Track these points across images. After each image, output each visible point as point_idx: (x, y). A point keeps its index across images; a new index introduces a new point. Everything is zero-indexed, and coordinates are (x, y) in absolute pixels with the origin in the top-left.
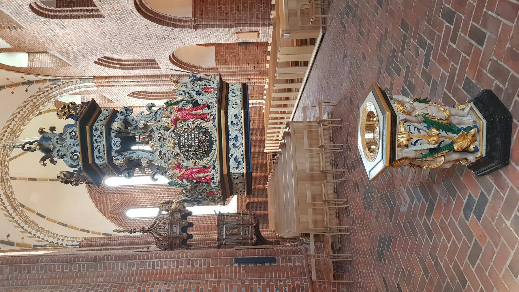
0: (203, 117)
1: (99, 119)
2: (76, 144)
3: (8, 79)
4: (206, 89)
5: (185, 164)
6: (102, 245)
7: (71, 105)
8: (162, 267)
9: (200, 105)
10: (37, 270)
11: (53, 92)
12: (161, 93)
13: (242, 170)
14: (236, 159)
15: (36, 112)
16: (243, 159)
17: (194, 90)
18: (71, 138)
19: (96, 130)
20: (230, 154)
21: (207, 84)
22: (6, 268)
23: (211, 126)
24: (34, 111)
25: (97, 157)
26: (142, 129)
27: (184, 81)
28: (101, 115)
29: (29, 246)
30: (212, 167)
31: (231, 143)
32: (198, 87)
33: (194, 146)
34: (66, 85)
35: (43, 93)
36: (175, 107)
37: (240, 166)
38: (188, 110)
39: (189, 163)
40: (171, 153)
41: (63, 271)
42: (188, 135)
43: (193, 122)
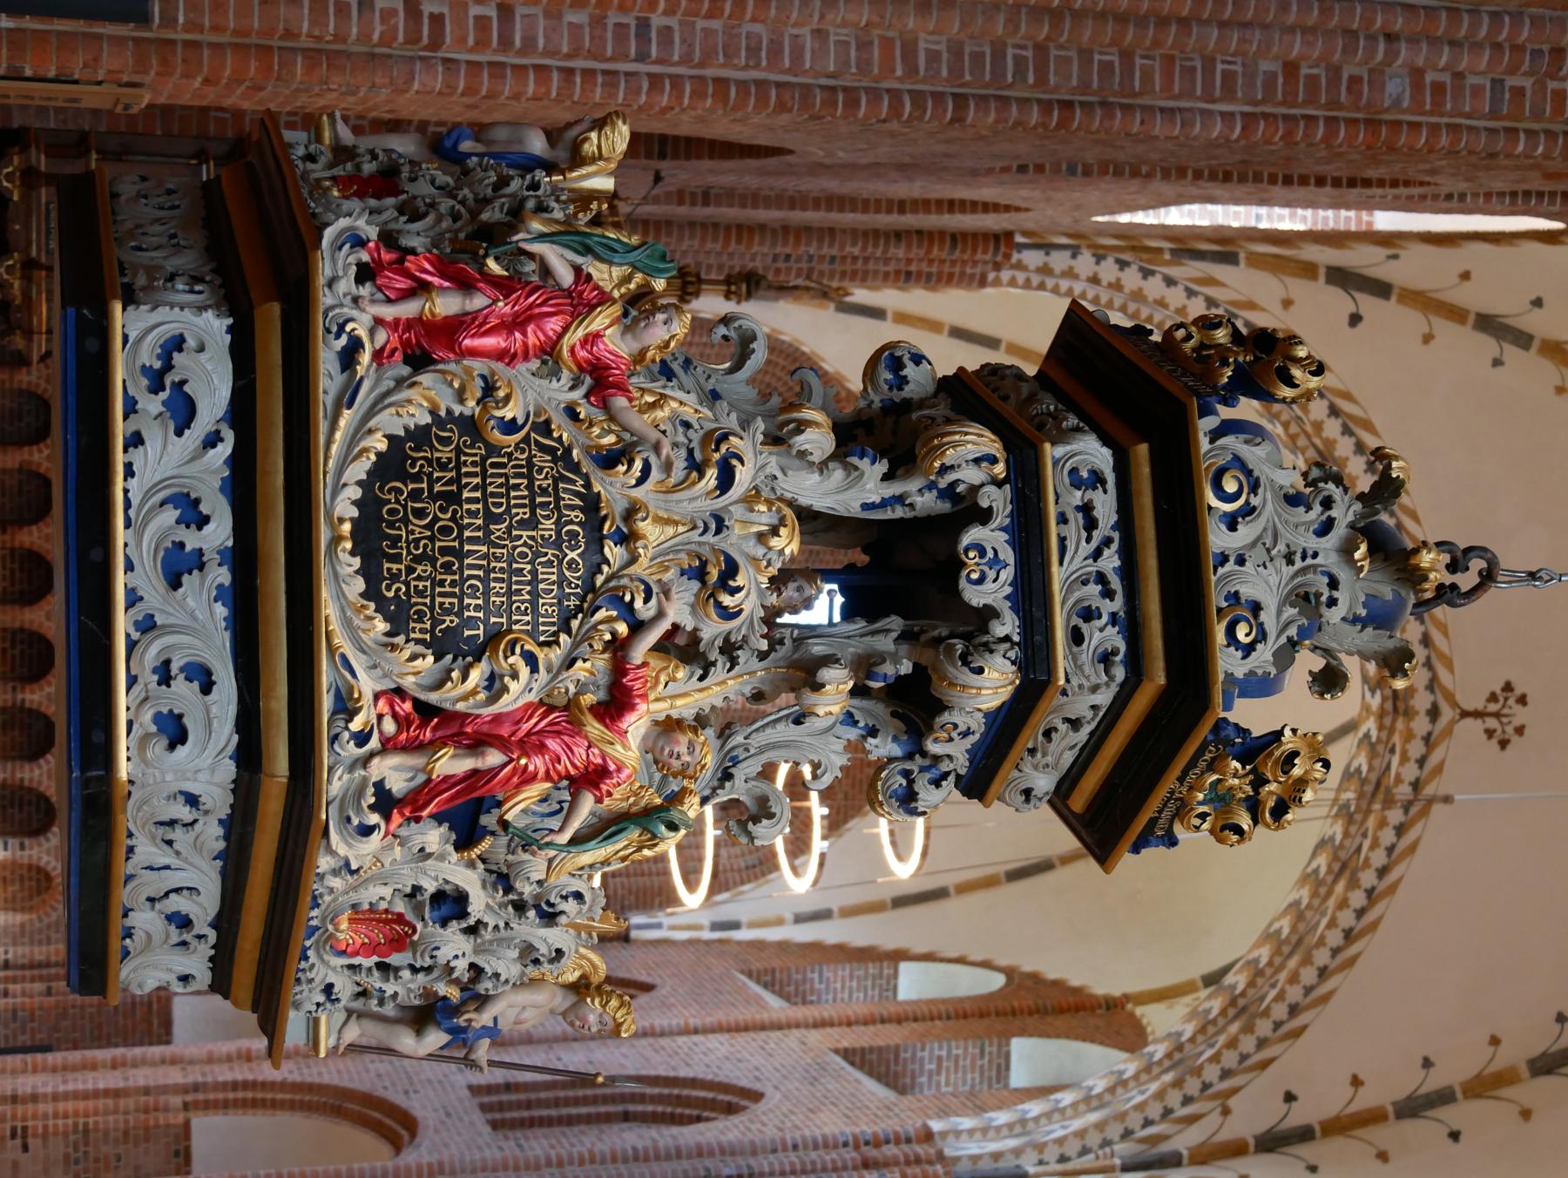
0: (427, 723)
1: (1083, 735)
2: (1230, 566)
3: (1383, 1156)
4: (392, 934)
5: (560, 391)
6: (899, 235)
7: (1245, 821)
8: (598, 22)
9: (439, 818)
10: (1250, 75)
11: (1160, 1095)
12: (570, 1121)
13: (136, 331)
14: (183, 412)
15: (1237, 979)
16: (131, 408)
17: (472, 931)
18: (1256, 608)
19: (1106, 658)
20: (225, 449)
21: (375, 981)
22: (1397, 102)
23: (365, 657)
24: (1251, 984)
25: (1103, 482)
26: (828, 660)
27: (539, 997)
28: (1068, 758)
29: (1257, 261)
30: (366, 357)
31: (219, 533)
32: (444, 955)
33: (491, 518)
34: (1093, 1140)
35: (1206, 1086)
36: (618, 797)
37: (149, 356)
38: (528, 778)
39: (531, 394)
40: (655, 474)
41: (1126, 56)
42: (535, 595)
43: (494, 686)
